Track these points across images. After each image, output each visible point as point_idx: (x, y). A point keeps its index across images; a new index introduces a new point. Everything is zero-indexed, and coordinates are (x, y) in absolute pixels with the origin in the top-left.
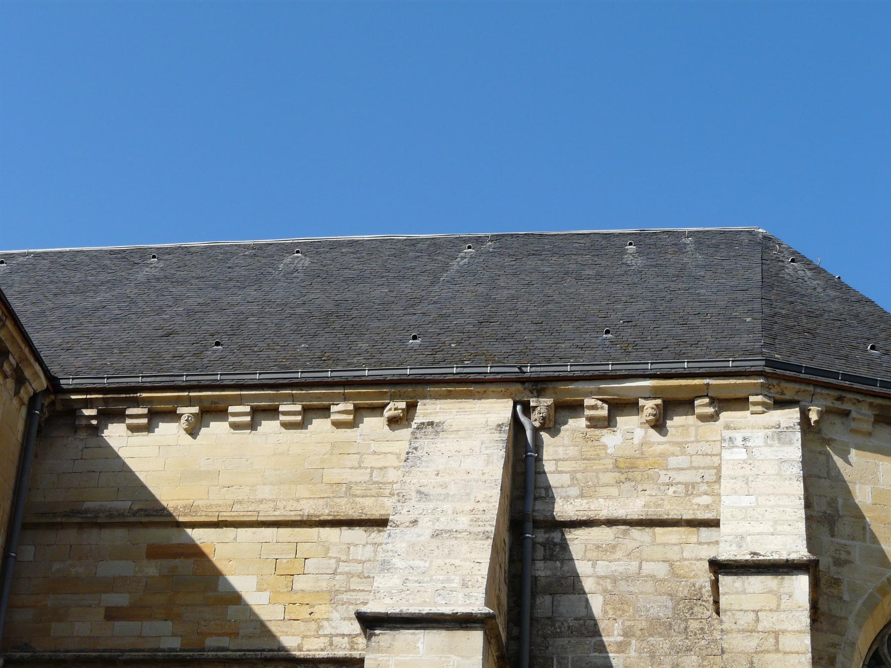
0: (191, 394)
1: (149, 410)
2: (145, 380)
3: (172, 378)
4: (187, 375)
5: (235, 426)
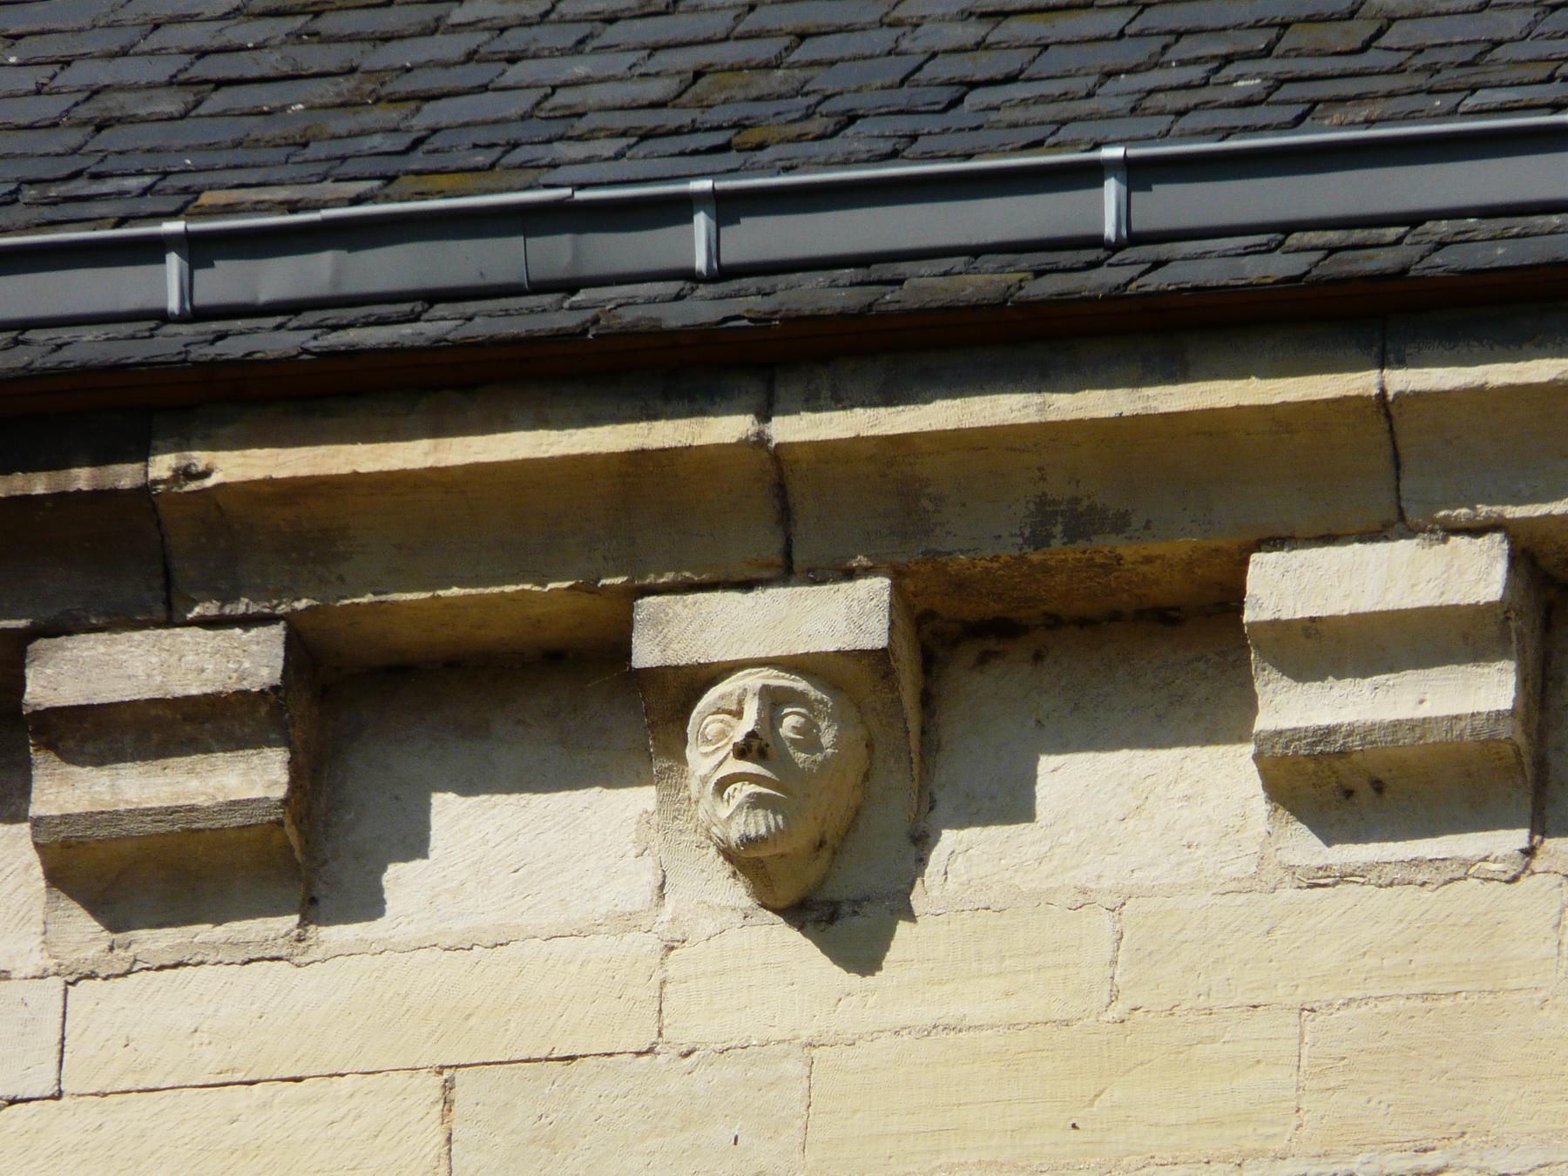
0: (790, 429)
1: (302, 650)
2: (225, 281)
3: (555, 253)
4: (728, 207)
5: (1336, 791)
